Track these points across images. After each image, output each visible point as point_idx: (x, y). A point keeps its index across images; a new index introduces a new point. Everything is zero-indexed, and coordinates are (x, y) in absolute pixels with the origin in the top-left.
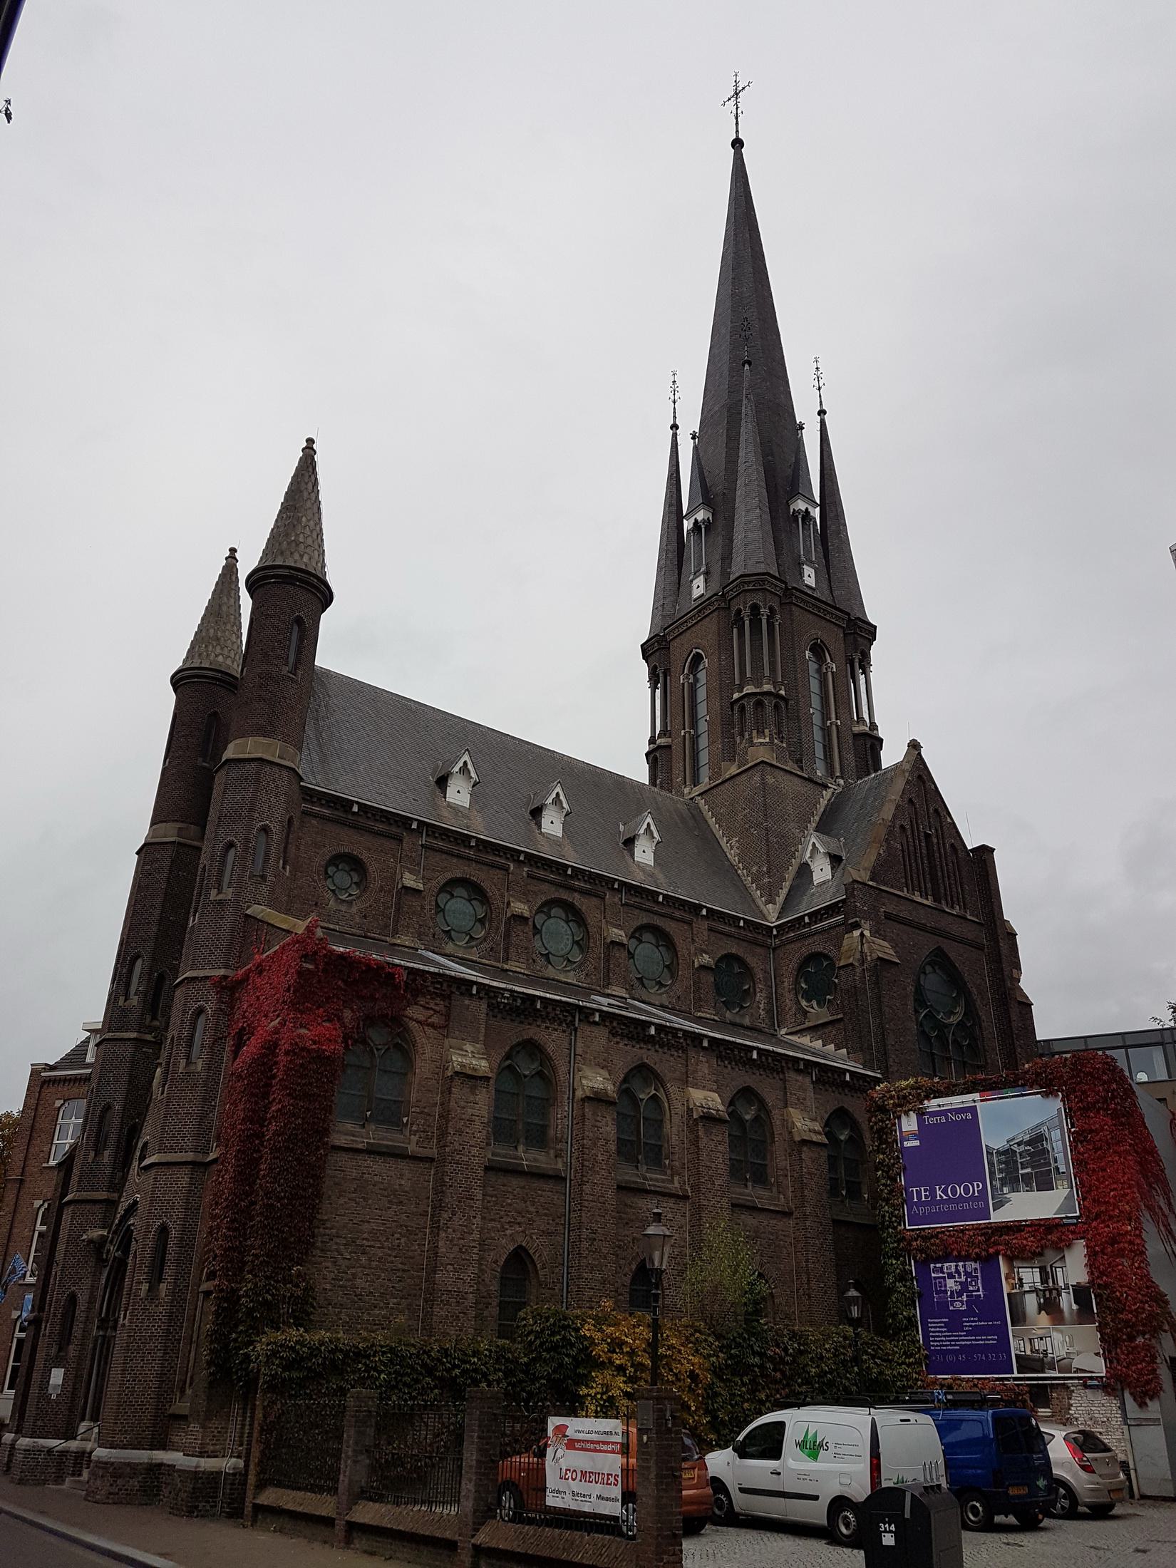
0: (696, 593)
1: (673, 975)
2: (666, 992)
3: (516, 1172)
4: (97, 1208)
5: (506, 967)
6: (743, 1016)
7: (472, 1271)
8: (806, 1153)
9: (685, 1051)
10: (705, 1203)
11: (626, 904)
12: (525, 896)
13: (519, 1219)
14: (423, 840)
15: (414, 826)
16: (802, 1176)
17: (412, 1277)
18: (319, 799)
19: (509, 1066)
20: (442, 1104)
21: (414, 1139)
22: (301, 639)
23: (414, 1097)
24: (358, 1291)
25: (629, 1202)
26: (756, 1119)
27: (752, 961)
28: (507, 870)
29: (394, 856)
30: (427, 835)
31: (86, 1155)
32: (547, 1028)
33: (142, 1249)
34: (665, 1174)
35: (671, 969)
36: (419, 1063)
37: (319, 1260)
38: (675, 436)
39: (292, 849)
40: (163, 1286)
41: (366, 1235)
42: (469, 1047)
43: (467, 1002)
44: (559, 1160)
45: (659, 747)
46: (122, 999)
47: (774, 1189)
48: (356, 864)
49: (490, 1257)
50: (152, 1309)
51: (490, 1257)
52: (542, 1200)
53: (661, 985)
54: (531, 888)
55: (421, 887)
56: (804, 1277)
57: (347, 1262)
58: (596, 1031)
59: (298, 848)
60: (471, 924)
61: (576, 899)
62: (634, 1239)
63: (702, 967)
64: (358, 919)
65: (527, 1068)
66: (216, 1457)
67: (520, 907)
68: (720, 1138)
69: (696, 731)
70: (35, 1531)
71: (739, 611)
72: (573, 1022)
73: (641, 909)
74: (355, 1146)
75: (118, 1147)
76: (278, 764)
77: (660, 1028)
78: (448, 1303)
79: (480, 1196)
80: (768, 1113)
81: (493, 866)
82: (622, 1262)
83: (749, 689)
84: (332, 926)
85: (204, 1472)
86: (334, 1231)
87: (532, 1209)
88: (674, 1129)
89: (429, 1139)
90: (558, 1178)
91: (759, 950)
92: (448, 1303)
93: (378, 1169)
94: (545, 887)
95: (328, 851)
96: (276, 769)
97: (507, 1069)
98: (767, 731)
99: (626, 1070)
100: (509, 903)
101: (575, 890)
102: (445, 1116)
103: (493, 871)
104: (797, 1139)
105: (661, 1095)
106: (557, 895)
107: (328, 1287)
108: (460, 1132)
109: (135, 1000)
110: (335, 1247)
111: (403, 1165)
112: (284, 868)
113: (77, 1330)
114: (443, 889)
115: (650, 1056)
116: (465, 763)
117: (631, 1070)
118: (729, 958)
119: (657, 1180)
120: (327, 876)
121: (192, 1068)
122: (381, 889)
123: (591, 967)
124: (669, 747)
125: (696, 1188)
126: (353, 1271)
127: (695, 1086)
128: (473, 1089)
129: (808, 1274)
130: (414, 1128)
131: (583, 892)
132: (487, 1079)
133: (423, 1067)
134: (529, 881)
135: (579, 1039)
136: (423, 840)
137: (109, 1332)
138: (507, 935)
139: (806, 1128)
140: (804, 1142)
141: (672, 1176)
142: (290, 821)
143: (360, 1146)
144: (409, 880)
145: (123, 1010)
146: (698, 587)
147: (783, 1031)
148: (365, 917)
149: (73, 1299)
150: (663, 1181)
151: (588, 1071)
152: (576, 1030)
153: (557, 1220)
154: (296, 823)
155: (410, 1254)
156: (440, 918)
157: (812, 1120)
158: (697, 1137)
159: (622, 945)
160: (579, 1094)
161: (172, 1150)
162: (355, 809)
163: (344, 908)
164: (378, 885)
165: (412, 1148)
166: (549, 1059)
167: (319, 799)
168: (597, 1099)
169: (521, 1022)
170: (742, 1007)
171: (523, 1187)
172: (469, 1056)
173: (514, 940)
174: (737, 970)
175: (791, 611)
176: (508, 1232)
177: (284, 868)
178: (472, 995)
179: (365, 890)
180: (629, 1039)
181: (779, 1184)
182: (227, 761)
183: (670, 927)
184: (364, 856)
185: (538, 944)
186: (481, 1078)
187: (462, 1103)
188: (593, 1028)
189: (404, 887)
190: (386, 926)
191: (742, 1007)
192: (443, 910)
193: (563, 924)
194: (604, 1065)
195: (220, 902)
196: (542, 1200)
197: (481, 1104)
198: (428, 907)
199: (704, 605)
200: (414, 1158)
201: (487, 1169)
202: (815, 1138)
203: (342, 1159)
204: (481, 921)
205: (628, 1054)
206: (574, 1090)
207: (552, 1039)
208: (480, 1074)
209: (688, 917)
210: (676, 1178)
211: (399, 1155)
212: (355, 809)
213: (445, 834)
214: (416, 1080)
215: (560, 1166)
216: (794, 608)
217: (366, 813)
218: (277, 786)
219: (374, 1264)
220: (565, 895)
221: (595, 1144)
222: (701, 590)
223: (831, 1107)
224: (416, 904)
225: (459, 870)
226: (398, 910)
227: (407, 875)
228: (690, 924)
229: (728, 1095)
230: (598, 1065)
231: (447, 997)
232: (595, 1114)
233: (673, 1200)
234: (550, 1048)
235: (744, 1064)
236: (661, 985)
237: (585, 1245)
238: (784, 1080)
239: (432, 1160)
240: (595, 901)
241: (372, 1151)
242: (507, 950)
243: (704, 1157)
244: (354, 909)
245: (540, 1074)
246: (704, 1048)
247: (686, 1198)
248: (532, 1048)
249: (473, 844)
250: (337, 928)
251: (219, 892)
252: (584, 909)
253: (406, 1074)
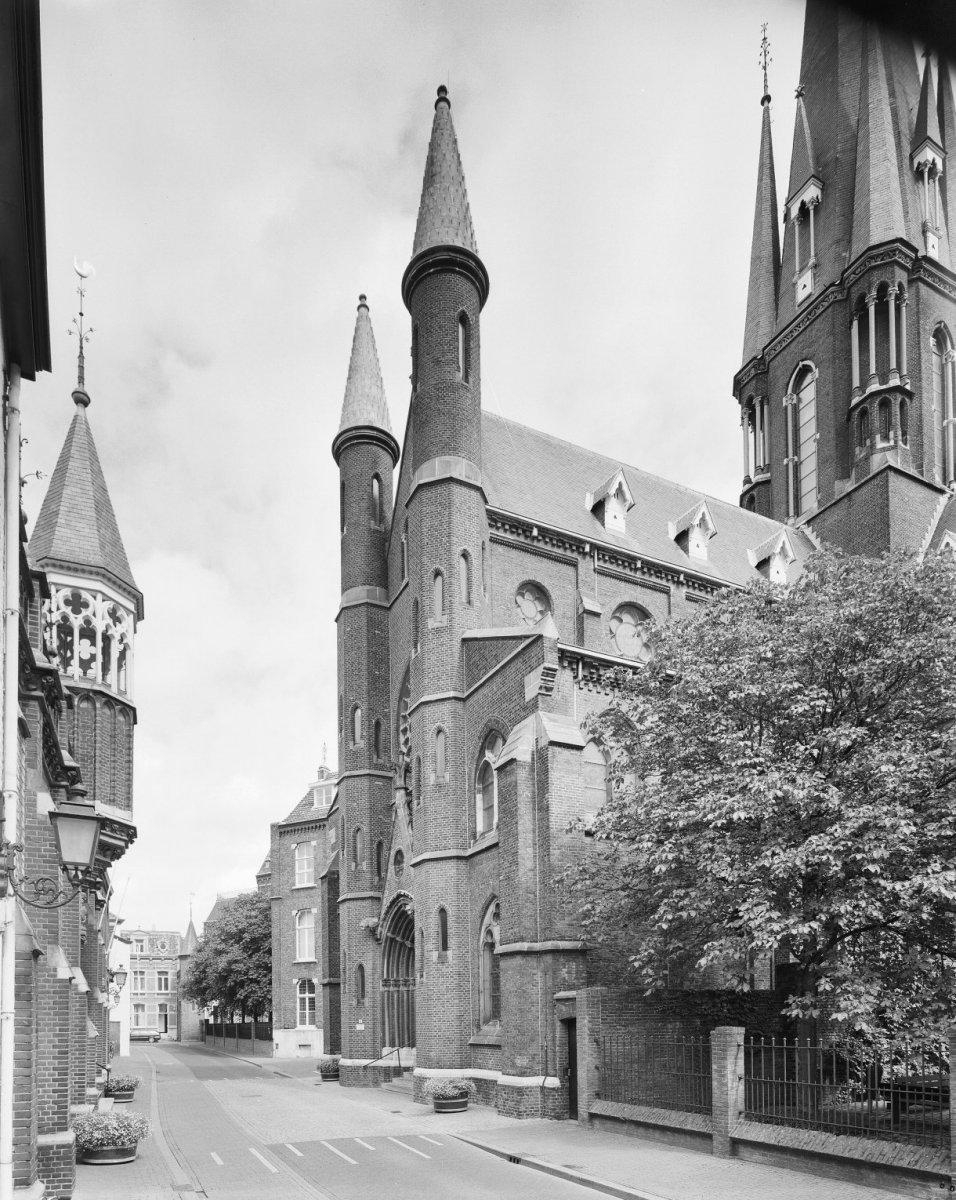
0: (801, 295)
4: (364, 903)
22: (467, 339)
30: (599, 559)
31: (349, 866)
33: (426, 925)
38: (766, 111)
40: (449, 953)
45: (758, 484)
46: (351, 743)
50: (444, 970)
69: (799, 458)
71: (862, 298)
75: (371, 859)
81: (654, 588)
83: (875, 387)
98: (892, 434)
109: (361, 743)
113: (368, 987)
116: (620, 484)
124: (767, 482)
137: (411, 988)
145: (355, 753)
146: (805, 286)
149: (361, 968)
161: (437, 848)
162: (535, 532)
167: (503, 525)
175: (918, 288)
182: (420, 487)
184: (546, 583)
199: (812, 306)
216: (921, 285)
217: (544, 537)
222: (808, 290)
249: (639, 565)
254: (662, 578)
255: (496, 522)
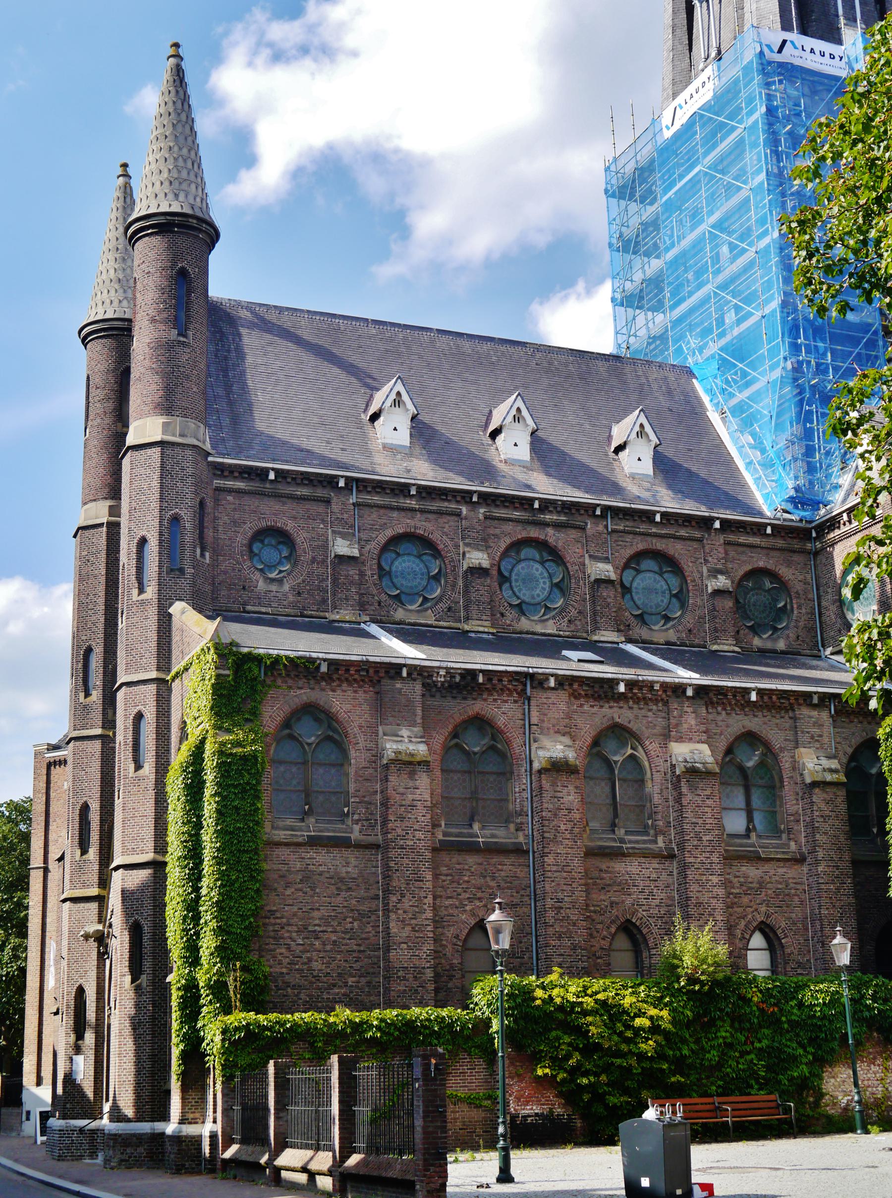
1: (683, 605)
2: (673, 626)
3: (471, 848)
5: (467, 628)
6: (775, 640)
7: (428, 947)
8: (818, 796)
9: (666, 703)
10: (692, 860)
11: (614, 531)
12: (484, 543)
13: (479, 895)
14: (353, 499)
15: (342, 483)
16: (812, 820)
17: (370, 957)
18: (232, 472)
19: (457, 745)
20: (382, 792)
21: (356, 828)
23: (352, 787)
24: (315, 973)
25: (604, 867)
26: (761, 764)
27: (786, 572)
28: (459, 515)
29: (323, 521)
30: (358, 491)
32: (495, 700)
34: (648, 835)
35: (681, 597)
36: (353, 753)
37: (272, 947)
39: (209, 533)
41: (317, 922)
42: (405, 732)
43: (398, 686)
44: (520, 834)
47: (784, 836)
48: (282, 537)
49: (450, 932)
51: (450, 932)
52: (503, 874)
53: (667, 619)
54: (491, 531)
55: (356, 553)
56: (818, 923)
57: (301, 948)
58: (553, 696)
59: (216, 530)
60: (424, 583)
61: (551, 535)
62: (612, 903)
63: (718, 592)
64: (291, 598)
65: (475, 744)
66: (196, 1123)
67: (478, 558)
68: (708, 792)
70: (56, 1193)
72: (524, 690)
73: (635, 533)
74: (295, 840)
76: (179, 444)
77: (631, 684)
78: (405, 979)
79: (429, 877)
80: (775, 756)
81: (440, 513)
82: (599, 926)
84: (263, 610)
85: (186, 1137)
86: (284, 920)
87: (493, 884)
88: (655, 787)
89: (373, 826)
90: (519, 851)
91: (796, 558)
92: (405, 979)
93: (325, 860)
94: (508, 527)
95: (249, 528)
96: (178, 450)
97: (454, 744)
99: (593, 733)
100: (464, 554)
101: (545, 524)
102: (385, 804)
103: (446, 518)
104: (808, 780)
105: (640, 754)
106: (524, 534)
107: (284, 970)
108: (402, 818)
110: (286, 935)
111: (347, 853)
112: (202, 555)
114: (385, 548)
115: (622, 714)
117: (601, 731)
118: (756, 573)
119: (637, 842)
120: (252, 554)
121: (141, 772)
122: (313, 560)
123: (574, 613)
125: (681, 846)
126: (308, 955)
127: (680, 739)
128: (412, 775)
129: (821, 920)
130: (356, 817)
131: (557, 526)
132: (426, 763)
133: (357, 757)
134: (488, 522)
135: (533, 708)
136: (353, 499)
138: (466, 592)
139: (818, 768)
140: (815, 784)
141: (656, 835)
142: (202, 504)
143: (300, 840)
144: (342, 547)
147: (829, 650)
148: (299, 594)
150: (645, 842)
151: (546, 741)
152: (529, 699)
153: (522, 892)
154: (209, 503)
155: (364, 936)
156: (386, 582)
157: (829, 758)
158: (680, 794)
159: (609, 582)
160: (536, 766)
161: (134, 851)
163: (274, 587)
164: (309, 557)
165: (356, 835)
166: (501, 732)
168: (558, 768)
169: (465, 698)
170: (775, 629)
171: (481, 864)
172: (405, 741)
173: (473, 596)
174: (768, 585)
176: (468, 908)
177: (202, 555)
178: (403, 679)
179: (295, 564)
180: (595, 699)
181: (789, 831)
183: (675, 549)
184: (290, 526)
185: (507, 593)
186: (419, 763)
187: (401, 790)
188: (550, 694)
189: (337, 556)
190: (324, 601)
191: (775, 629)
192: (389, 573)
193: (537, 566)
194: (568, 731)
195: (142, 602)
196: (503, 874)
197: (423, 788)
198: (369, 573)
200: (359, 846)
201: (434, 850)
202: (829, 777)
203: (283, 853)
204: (436, 578)
205: (593, 717)
206: (531, 762)
207: (503, 712)
208: (418, 759)
209: (697, 534)
210: (660, 839)
211: (342, 843)
212: (272, 476)
213: (380, 487)
214: (352, 771)
215: (521, 839)
218: (183, 469)
219: (328, 948)
220: (534, 533)
221: (555, 815)
223: (856, 741)
224: (353, 572)
225: (401, 524)
226: (335, 581)
227: (339, 541)
228: (700, 540)
229: (722, 745)
230: (558, 732)
231: (375, 683)
232: (554, 784)
233: (656, 861)
234: (501, 721)
235: (743, 707)
236: (667, 619)
237: (550, 914)
238: (794, 719)
239: (378, 846)
240: (573, 534)
241: (314, 842)
242: (466, 608)
243: (689, 814)
244: (286, 587)
245: (492, 748)
246: (689, 698)
247: (672, 856)
248: (481, 723)
249: (413, 492)
250: (270, 610)
251: (141, 591)
252: (560, 544)
253: (342, 765)
254: (449, 501)
255: (222, 471)
